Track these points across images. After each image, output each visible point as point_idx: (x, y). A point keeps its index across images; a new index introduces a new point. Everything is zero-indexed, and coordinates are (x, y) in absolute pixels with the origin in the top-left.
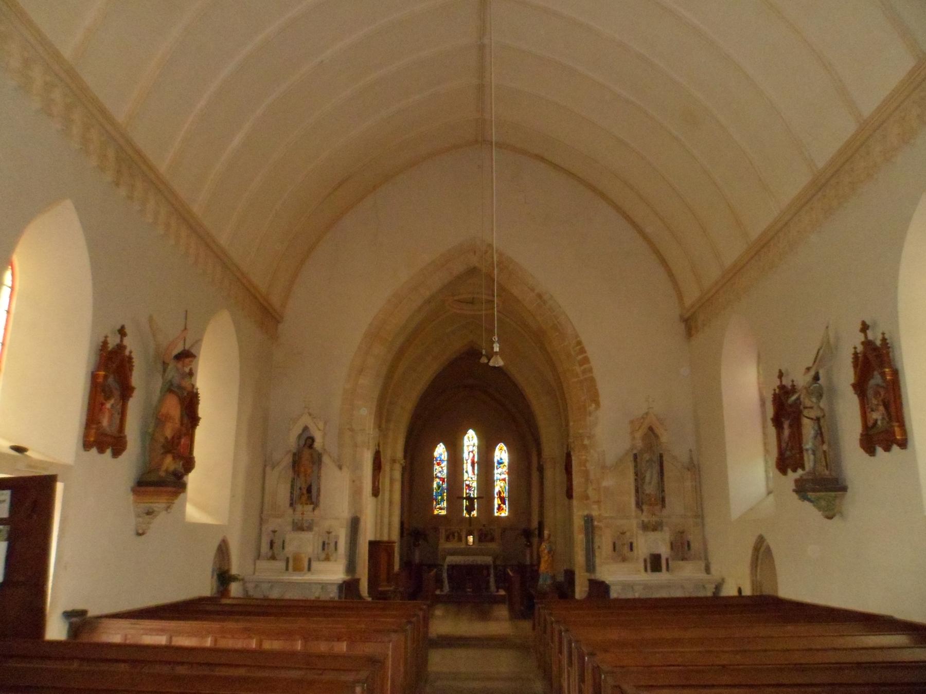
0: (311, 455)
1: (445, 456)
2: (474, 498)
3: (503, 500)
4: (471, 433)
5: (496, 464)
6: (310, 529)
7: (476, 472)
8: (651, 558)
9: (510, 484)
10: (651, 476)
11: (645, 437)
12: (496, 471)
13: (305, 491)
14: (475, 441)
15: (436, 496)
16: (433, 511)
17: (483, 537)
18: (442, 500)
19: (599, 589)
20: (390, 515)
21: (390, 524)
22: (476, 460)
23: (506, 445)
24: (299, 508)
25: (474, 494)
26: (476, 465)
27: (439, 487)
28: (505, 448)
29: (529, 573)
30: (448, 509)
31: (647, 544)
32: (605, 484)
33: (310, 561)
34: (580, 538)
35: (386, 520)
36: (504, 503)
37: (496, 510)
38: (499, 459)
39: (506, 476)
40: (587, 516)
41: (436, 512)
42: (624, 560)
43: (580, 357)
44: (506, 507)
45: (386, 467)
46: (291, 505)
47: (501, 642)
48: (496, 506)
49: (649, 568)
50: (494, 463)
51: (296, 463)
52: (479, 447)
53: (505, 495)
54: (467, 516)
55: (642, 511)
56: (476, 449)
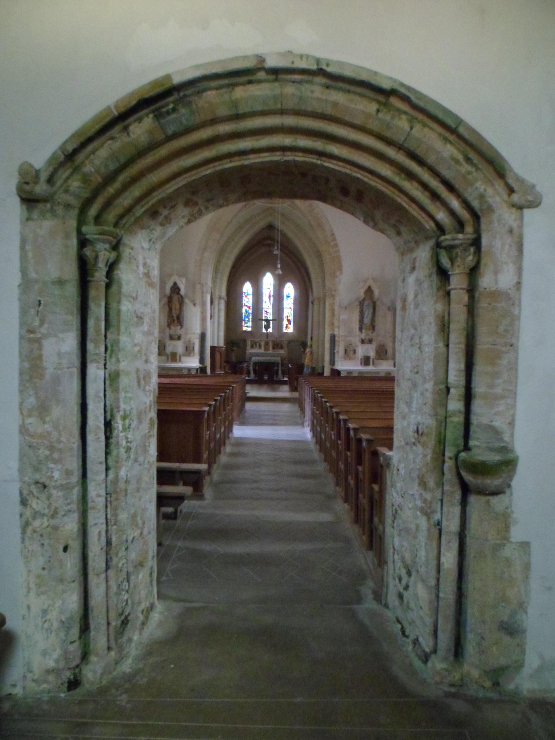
2: (270, 320)
3: (289, 321)
5: (285, 297)
6: (179, 338)
8: (364, 359)
10: (368, 314)
16: (242, 328)
18: (249, 321)
19: (336, 373)
20: (218, 332)
22: (272, 294)
24: (173, 327)
25: (270, 317)
27: (246, 312)
29: (300, 368)
30: (253, 327)
31: (361, 351)
34: (327, 345)
37: (284, 328)
38: (288, 294)
40: (332, 334)
41: (244, 329)
43: (332, 243)
44: (291, 327)
45: (216, 302)
47: (283, 400)
48: (285, 326)
53: (291, 318)
54: (265, 332)
55: (362, 332)
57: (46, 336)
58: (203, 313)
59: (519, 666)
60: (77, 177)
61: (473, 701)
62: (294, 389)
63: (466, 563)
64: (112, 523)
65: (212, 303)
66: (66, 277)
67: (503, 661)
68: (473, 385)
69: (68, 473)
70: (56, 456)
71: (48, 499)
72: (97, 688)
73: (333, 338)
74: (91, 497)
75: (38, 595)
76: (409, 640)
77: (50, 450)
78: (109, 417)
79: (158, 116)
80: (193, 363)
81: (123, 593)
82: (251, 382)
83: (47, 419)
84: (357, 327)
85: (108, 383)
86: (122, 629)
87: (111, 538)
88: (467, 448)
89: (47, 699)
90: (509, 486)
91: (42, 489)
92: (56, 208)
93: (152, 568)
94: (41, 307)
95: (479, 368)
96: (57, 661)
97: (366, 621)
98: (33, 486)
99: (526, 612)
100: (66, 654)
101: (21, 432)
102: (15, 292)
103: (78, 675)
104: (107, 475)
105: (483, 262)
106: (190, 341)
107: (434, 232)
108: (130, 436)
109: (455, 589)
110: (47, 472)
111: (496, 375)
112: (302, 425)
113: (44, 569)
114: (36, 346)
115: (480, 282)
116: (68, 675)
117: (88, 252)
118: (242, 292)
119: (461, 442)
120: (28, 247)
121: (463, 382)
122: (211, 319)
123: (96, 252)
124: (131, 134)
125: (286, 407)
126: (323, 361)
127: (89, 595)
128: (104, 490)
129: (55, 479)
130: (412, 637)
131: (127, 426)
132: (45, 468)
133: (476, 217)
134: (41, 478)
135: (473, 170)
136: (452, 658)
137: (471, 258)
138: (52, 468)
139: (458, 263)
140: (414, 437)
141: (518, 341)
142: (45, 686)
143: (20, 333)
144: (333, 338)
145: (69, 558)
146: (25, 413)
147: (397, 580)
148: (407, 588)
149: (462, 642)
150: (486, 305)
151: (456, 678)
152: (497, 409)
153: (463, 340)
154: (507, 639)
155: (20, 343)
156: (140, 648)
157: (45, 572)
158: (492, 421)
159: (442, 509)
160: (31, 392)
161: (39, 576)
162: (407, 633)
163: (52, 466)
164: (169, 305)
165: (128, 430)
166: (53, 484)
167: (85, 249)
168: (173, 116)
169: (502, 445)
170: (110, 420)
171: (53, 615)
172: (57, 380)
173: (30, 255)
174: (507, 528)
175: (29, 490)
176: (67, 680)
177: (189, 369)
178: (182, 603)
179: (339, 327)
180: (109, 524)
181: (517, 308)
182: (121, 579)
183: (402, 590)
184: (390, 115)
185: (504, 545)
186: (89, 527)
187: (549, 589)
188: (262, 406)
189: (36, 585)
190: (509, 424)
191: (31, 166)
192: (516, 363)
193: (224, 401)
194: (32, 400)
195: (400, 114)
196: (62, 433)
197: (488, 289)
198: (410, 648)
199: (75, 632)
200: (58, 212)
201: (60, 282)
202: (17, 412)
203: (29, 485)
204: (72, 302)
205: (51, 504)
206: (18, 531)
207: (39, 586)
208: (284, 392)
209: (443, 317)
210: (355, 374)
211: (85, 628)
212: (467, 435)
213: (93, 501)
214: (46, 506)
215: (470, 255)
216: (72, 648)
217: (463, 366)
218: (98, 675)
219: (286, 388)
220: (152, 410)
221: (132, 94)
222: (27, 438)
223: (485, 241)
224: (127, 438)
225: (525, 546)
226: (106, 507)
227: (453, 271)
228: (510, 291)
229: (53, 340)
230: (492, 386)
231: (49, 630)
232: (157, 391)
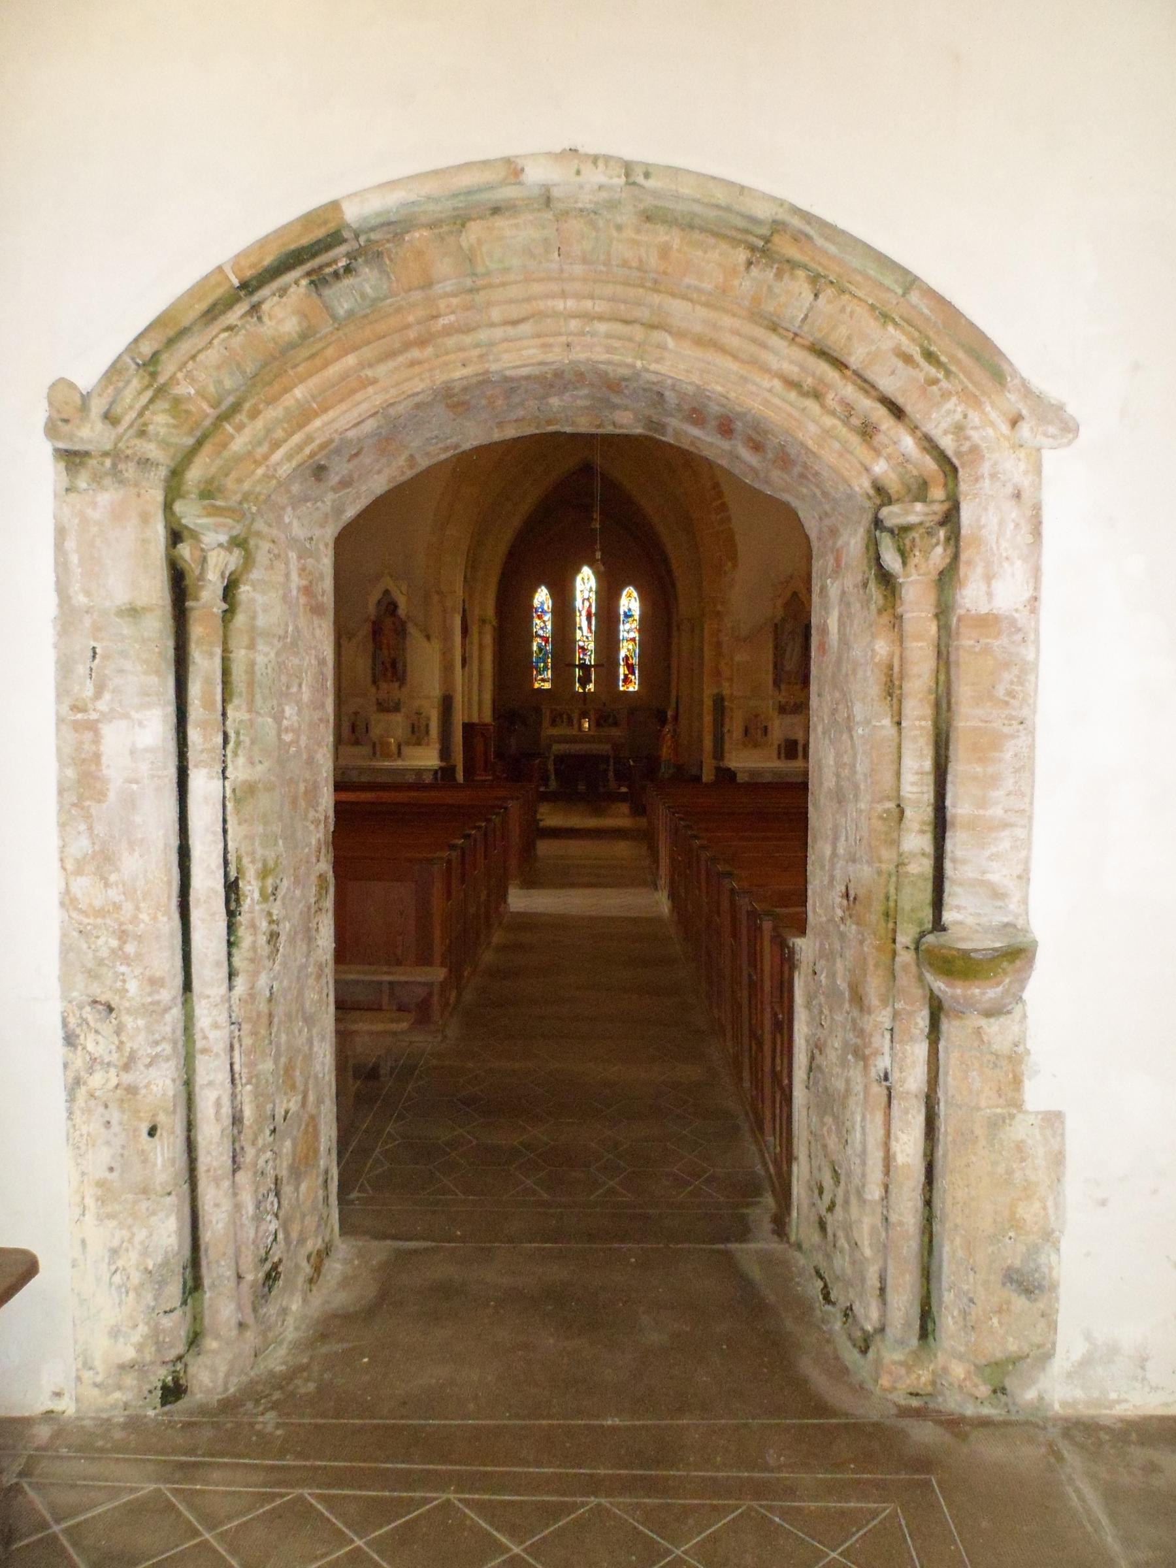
0: (394, 624)
1: (549, 605)
2: (591, 666)
3: (631, 668)
4: (586, 572)
5: (622, 618)
6: (396, 708)
7: (593, 628)
9: (642, 645)
11: (787, 605)
12: (621, 627)
13: (388, 665)
14: (593, 583)
15: (537, 662)
16: (533, 685)
17: (601, 721)
18: (545, 668)
19: (726, 776)
21: (480, 703)
22: (593, 610)
23: (636, 588)
25: (590, 659)
26: (593, 619)
27: (540, 649)
28: (635, 594)
29: (651, 765)
30: (553, 680)
32: (737, 658)
33: (399, 746)
34: (708, 719)
35: (475, 698)
36: (633, 673)
37: (621, 683)
39: (635, 635)
40: (718, 694)
41: (536, 686)
42: (756, 746)
44: (635, 678)
45: (474, 629)
46: (374, 682)
48: (622, 677)
49: (783, 755)
50: (619, 615)
51: (377, 631)
52: (597, 593)
53: (635, 661)
55: (780, 690)
56: (593, 596)
57: (108, 717)
58: (446, 652)
59: (1046, 1356)
60: (162, 404)
61: (954, 1424)
62: (639, 810)
63: (940, 1152)
64: (244, 1081)
65: (465, 631)
66: (141, 601)
67: (1013, 1346)
68: (948, 803)
69: (155, 983)
70: (130, 948)
71: (118, 1033)
72: (219, 1401)
73: (719, 703)
74: (202, 1030)
75: (100, 1219)
76: (835, 1312)
77: (120, 938)
78: (233, 874)
79: (319, 281)
80: (427, 758)
81: (269, 1218)
82: (544, 797)
83: (113, 878)
84: (770, 678)
85: (230, 806)
86: (266, 1289)
87: (241, 1111)
88: (938, 925)
89: (122, 1420)
90: (1020, 999)
91: (104, 1014)
92: (121, 466)
93: (327, 1172)
94: (97, 661)
95: (958, 769)
96: (140, 1348)
97: (756, 1273)
98: (88, 1009)
99: (1058, 1250)
100: (156, 1336)
101: (62, 904)
102: (47, 634)
103: (182, 1374)
104: (231, 988)
105: (964, 557)
106: (419, 713)
107: (869, 498)
108: (275, 912)
109: (920, 1204)
110: (115, 982)
111: (994, 781)
112: (655, 887)
113: (111, 1169)
114: (88, 736)
115: (958, 597)
116: (162, 1374)
117: (185, 550)
118: (532, 606)
119: (927, 914)
120: (71, 544)
121: (929, 796)
122: (463, 666)
123: (202, 550)
124: (265, 319)
125: (622, 849)
126: (701, 750)
127: (201, 1225)
128: (225, 1015)
129: (129, 995)
130: (843, 1303)
131: (270, 890)
132: (110, 974)
133: (949, 468)
134: (102, 992)
135: (941, 375)
136: (914, 1342)
137: (939, 550)
138: (123, 974)
139: (916, 560)
140: (841, 906)
141: (1034, 713)
142: (117, 1395)
143: (57, 713)
144: (719, 703)
145: (159, 1148)
146: (70, 866)
147: (816, 1192)
148: (831, 1208)
149: (934, 1309)
150: (971, 642)
151: (923, 1379)
152: (993, 849)
153: (928, 711)
154: (1020, 1302)
155: (58, 730)
156: (303, 1327)
157: (115, 1175)
158: (984, 873)
159: (892, 1048)
160: (82, 827)
161: (101, 1184)
162: (833, 1297)
163: (123, 969)
164: (374, 639)
165: (272, 898)
166: (127, 1004)
167: (180, 546)
168: (348, 282)
169: (1006, 920)
170: (237, 879)
171: (130, 1259)
172: (130, 802)
173: (74, 559)
174: (1017, 1082)
175: (81, 1017)
176: (160, 1385)
177: (419, 772)
178: (388, 1242)
179: (731, 679)
180: (238, 1081)
181: (1032, 649)
182: (263, 1190)
183: (823, 1213)
184: (774, 270)
185: (1012, 1117)
186: (197, 1089)
187: (1103, 1203)
188: (574, 848)
189: (97, 1200)
190: (1019, 877)
191: (72, 386)
192: (1031, 758)
193: (486, 835)
194: (82, 845)
195: (793, 268)
196: (142, 905)
197: (973, 612)
198: (838, 1326)
199: (174, 1289)
200: (126, 475)
201: (133, 612)
202: (56, 865)
203: (81, 1008)
204: (157, 650)
205: (122, 1043)
206: (62, 1096)
207: (101, 1200)
208: (619, 818)
209: (891, 668)
210: (768, 778)
211: (194, 1285)
212: (938, 903)
213: (205, 1038)
214: (113, 1047)
215: (937, 544)
216: (167, 1322)
217: (928, 764)
218: (221, 1375)
219: (624, 808)
220: (322, 858)
221: (263, 243)
222: (74, 915)
223: (967, 515)
224: (270, 914)
225: (1053, 1120)
226: (232, 1047)
227: (908, 576)
228: (1016, 615)
229: (123, 724)
230: (982, 803)
231: (124, 1289)
232: (332, 820)
